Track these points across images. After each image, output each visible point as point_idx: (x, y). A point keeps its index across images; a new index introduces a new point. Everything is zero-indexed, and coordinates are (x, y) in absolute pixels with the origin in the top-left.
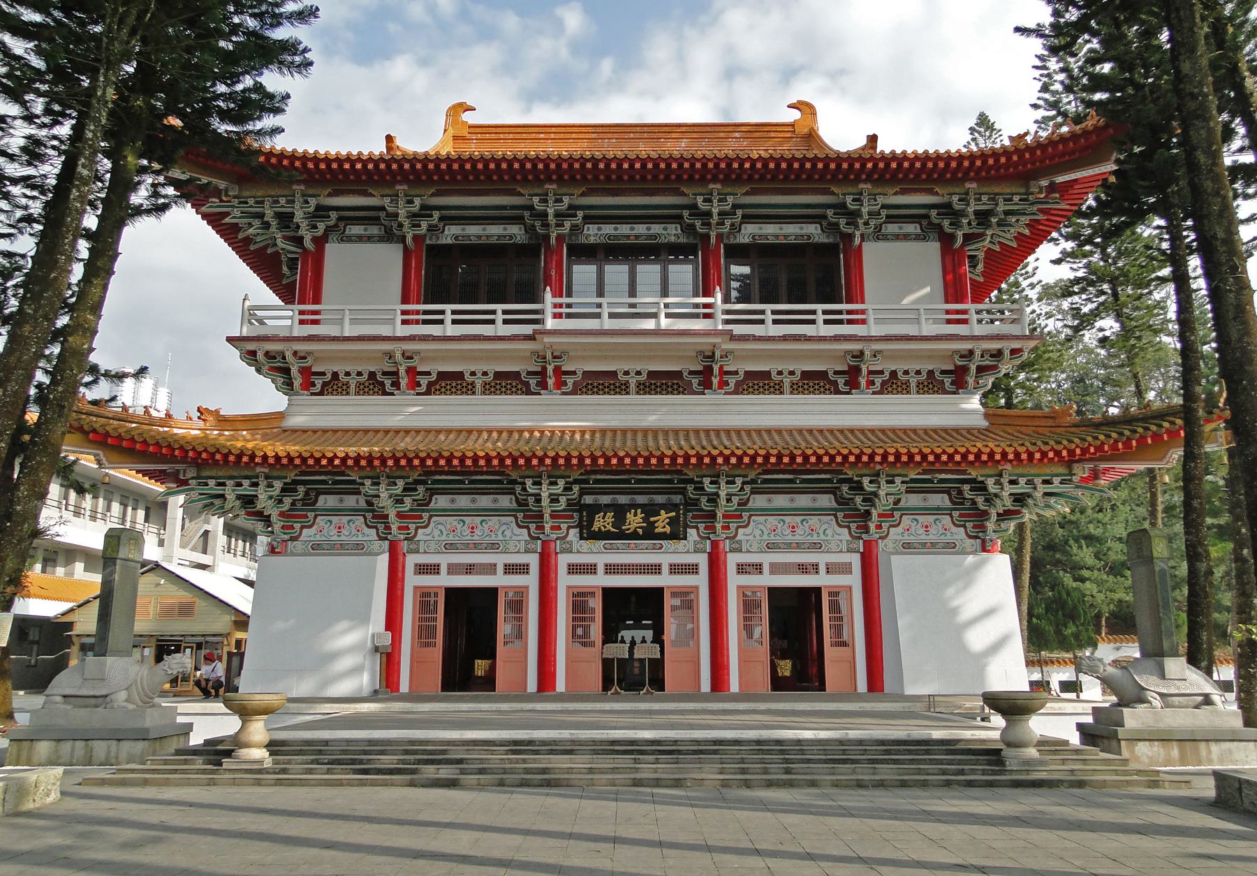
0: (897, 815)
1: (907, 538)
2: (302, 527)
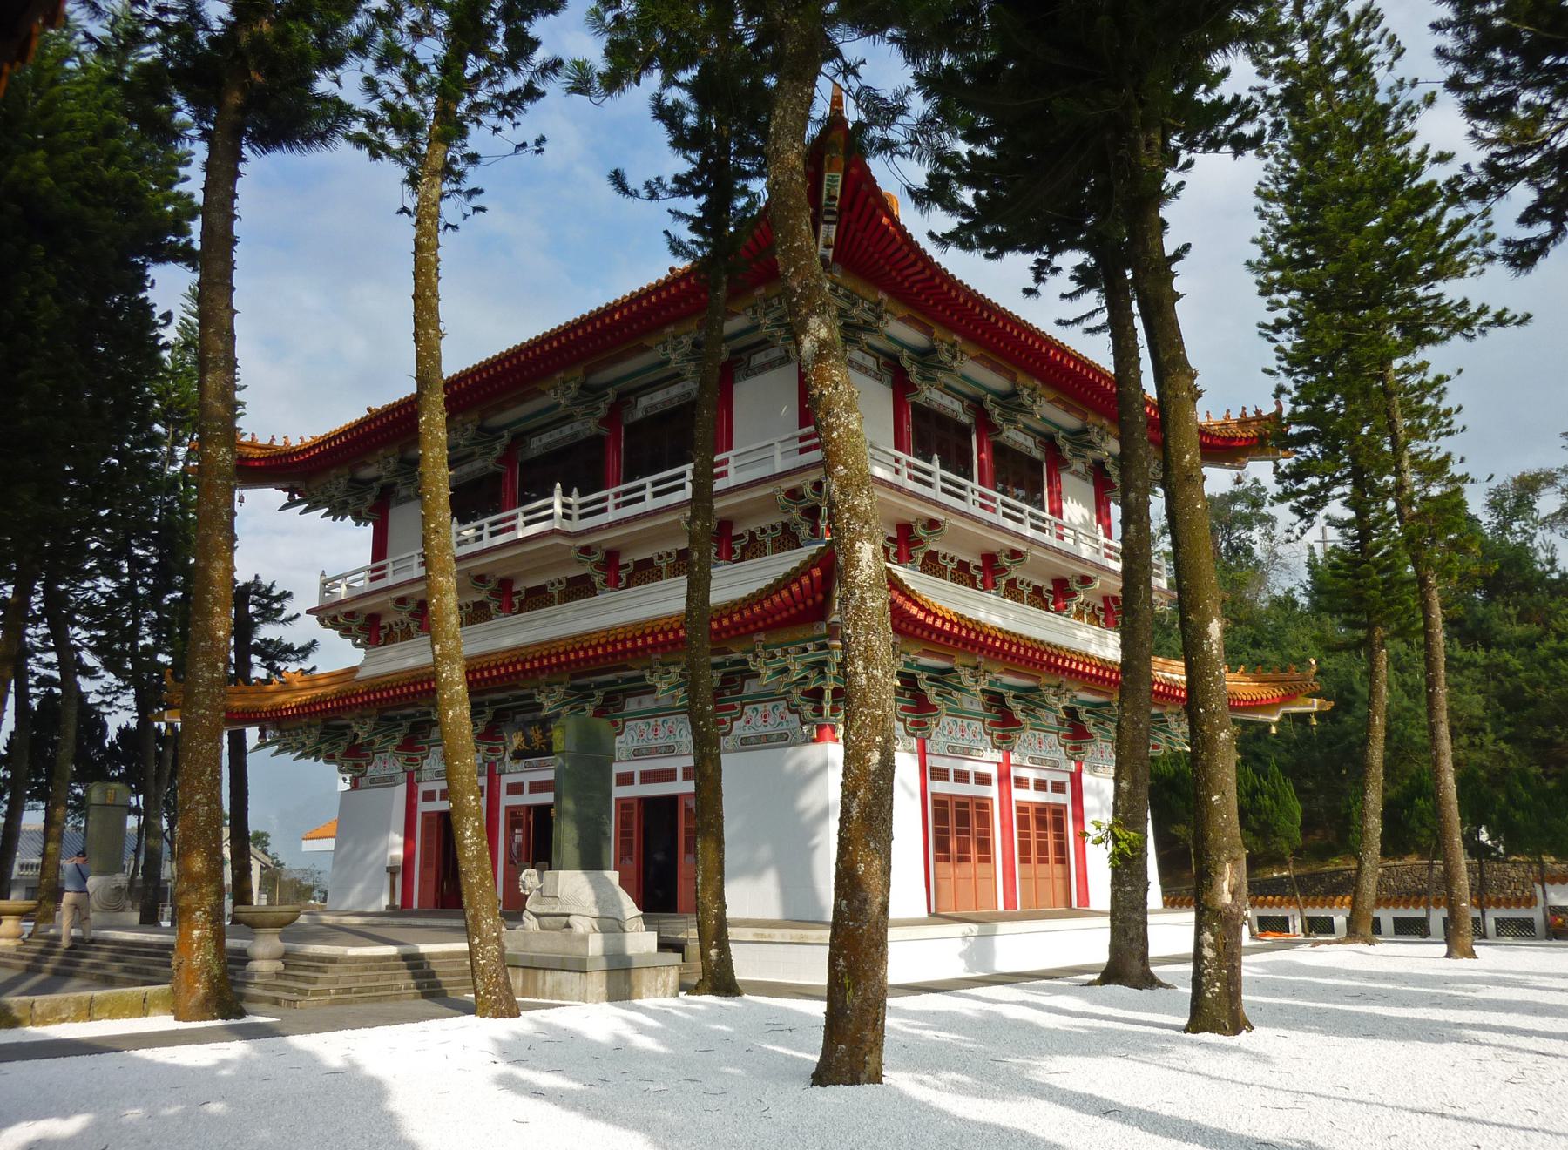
0: (409, 926)
1: (748, 732)
2: (732, 720)
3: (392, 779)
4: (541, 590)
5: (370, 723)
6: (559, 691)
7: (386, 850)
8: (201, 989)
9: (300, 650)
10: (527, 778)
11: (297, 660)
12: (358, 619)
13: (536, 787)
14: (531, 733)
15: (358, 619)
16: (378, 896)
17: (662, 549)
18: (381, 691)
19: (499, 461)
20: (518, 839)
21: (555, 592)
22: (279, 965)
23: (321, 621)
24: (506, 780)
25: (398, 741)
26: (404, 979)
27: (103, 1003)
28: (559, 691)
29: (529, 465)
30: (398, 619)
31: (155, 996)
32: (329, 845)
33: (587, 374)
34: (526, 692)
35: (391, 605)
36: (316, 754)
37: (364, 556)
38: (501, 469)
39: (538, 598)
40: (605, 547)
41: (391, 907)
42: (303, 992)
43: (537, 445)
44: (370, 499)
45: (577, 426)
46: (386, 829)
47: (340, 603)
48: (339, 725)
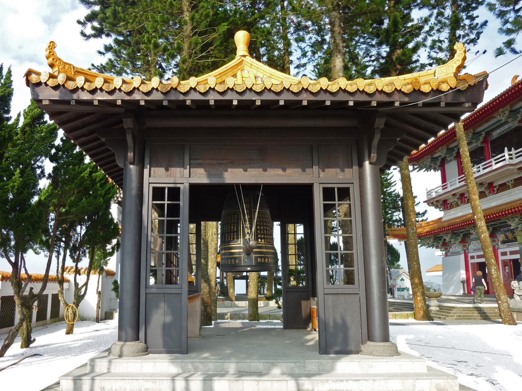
3: (459, 252)
4: (505, 184)
5: (449, 236)
6: (517, 220)
7: (460, 275)
8: (422, 313)
9: (422, 214)
10: (508, 250)
11: (422, 217)
12: (442, 203)
13: (512, 253)
14: (508, 234)
15: (442, 203)
16: (459, 290)
17: (509, 179)
18: (452, 226)
19: (482, 143)
20: (507, 271)
21: (510, 184)
22: (438, 309)
23: (428, 204)
24: (500, 251)
25: (460, 240)
26: (476, 314)
27: (398, 315)
28: (517, 220)
29: (493, 142)
30: (453, 200)
31: (410, 314)
32: (441, 273)
33: (511, 107)
34: (504, 221)
35: (451, 197)
36: (433, 246)
37: (439, 182)
38: (483, 145)
39: (503, 187)
40: (488, 182)
41: (464, 294)
42: (448, 316)
43: (495, 134)
44: (438, 163)
45: (510, 125)
46: (459, 269)
47: (434, 198)
48: (438, 236)
